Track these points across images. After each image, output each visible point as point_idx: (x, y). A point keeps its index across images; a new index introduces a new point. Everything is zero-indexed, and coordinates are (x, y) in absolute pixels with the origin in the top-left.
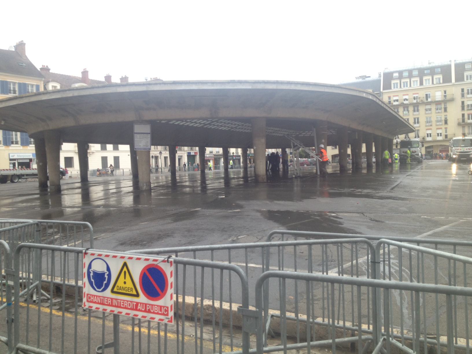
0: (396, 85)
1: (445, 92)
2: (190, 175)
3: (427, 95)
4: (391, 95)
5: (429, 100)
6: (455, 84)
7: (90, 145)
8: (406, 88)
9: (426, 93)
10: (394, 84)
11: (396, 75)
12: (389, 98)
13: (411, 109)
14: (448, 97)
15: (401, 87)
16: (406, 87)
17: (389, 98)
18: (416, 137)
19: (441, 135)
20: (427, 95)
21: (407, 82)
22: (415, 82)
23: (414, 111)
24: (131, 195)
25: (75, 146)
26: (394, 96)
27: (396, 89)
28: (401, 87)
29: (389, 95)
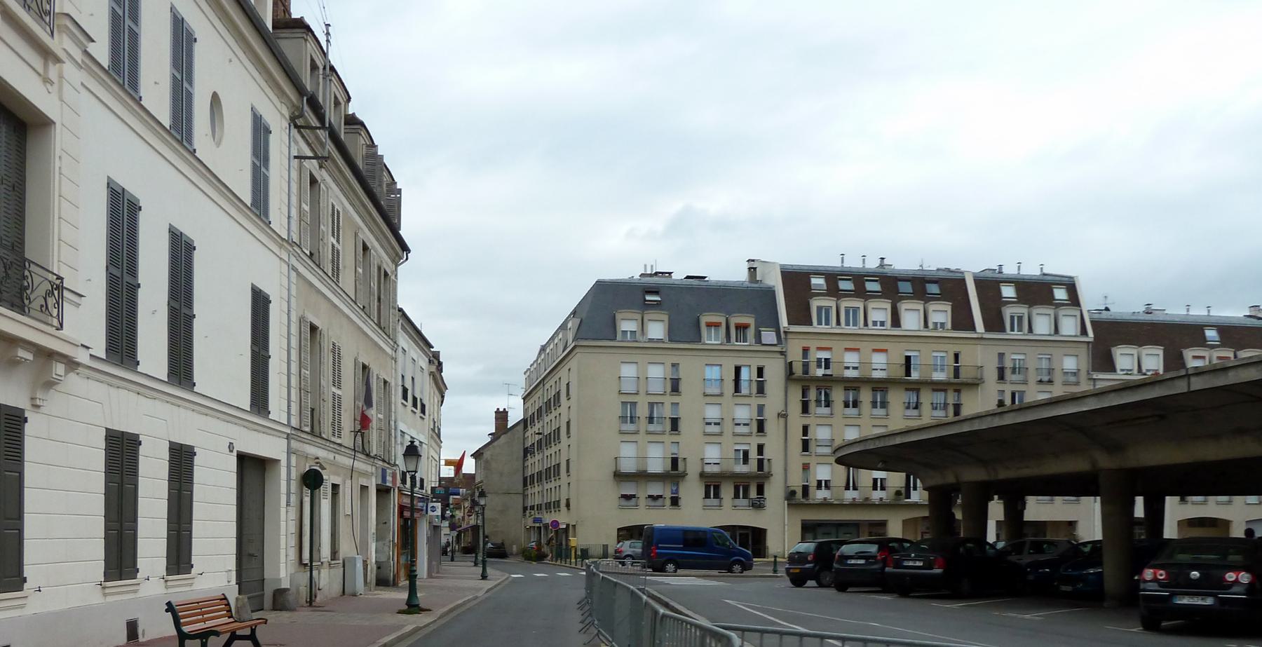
0: (824, 313)
1: (956, 356)
2: (737, 568)
3: (908, 359)
4: (813, 344)
5: (915, 375)
6: (985, 336)
7: (1244, 536)
8: (851, 329)
9: (908, 354)
10: (819, 309)
11: (817, 281)
12: (806, 351)
13: (866, 396)
14: (965, 375)
15: (838, 323)
16: (823, 326)
17: (806, 351)
18: (847, 488)
19: (883, 488)
20: (908, 359)
21: (828, 310)
22: (55, 277)
23: (874, 404)
24: (56, 364)
25: (1038, 502)
26: (819, 349)
27: (823, 328)
28: (838, 323)
29: (806, 344)
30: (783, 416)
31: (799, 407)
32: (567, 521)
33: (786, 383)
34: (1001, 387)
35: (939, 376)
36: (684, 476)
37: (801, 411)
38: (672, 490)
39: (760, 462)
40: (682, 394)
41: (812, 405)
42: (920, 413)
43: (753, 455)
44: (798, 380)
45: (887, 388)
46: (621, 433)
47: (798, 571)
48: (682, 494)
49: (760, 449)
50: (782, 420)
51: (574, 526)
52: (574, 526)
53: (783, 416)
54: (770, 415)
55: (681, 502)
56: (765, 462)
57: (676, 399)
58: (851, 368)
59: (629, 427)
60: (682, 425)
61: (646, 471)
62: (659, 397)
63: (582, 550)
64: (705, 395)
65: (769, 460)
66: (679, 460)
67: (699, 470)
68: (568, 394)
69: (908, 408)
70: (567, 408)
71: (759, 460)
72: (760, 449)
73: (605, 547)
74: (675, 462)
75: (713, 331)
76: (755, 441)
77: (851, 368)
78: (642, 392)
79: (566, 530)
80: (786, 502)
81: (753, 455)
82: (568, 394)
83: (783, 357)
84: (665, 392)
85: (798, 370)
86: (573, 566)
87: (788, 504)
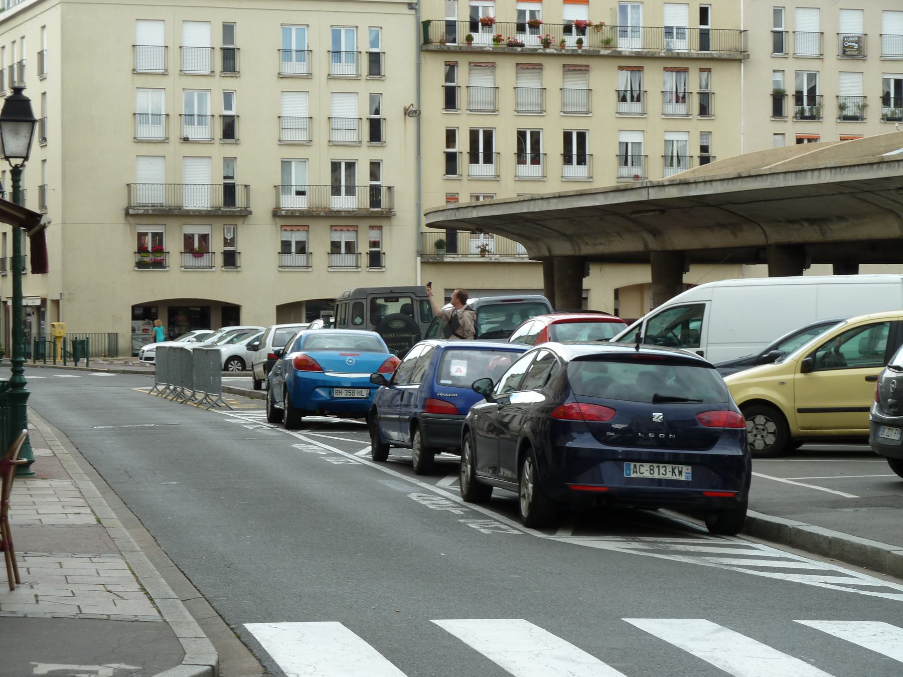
30: (413, 113)
31: (440, 97)
32: (42, 293)
33: (419, 58)
34: (779, 64)
35: (680, 46)
36: (245, 216)
37: (444, 172)
38: (225, 239)
39: (375, 191)
40: (242, 74)
41: (463, 161)
42: (643, 108)
43: (362, 177)
44: (441, 51)
45: (588, 66)
46: (281, 76)
47: (442, 453)
48: (241, 246)
49: (375, 168)
50: (411, 122)
51: (56, 303)
52: (56, 303)
53: (413, 113)
54: (391, 113)
55: (241, 260)
56: (384, 191)
57: (229, 84)
58: (806, 141)
59: (295, 67)
60: (241, 130)
61: (180, 208)
62: (203, 80)
63: (75, 343)
64: (137, 141)
65: (389, 188)
66: (237, 188)
67: (271, 205)
68: (41, 71)
69: (624, 99)
70: (40, 96)
71: (377, 179)
72: (375, 168)
73: (113, 337)
74: (229, 191)
75: (742, 67)
76: (363, 157)
77: (806, 141)
78: (174, 70)
79: (40, 311)
80: (419, 259)
81: (362, 177)
82: (41, 71)
83: (413, 12)
84: (213, 72)
85: (437, 32)
86: (61, 365)
87: (422, 263)
